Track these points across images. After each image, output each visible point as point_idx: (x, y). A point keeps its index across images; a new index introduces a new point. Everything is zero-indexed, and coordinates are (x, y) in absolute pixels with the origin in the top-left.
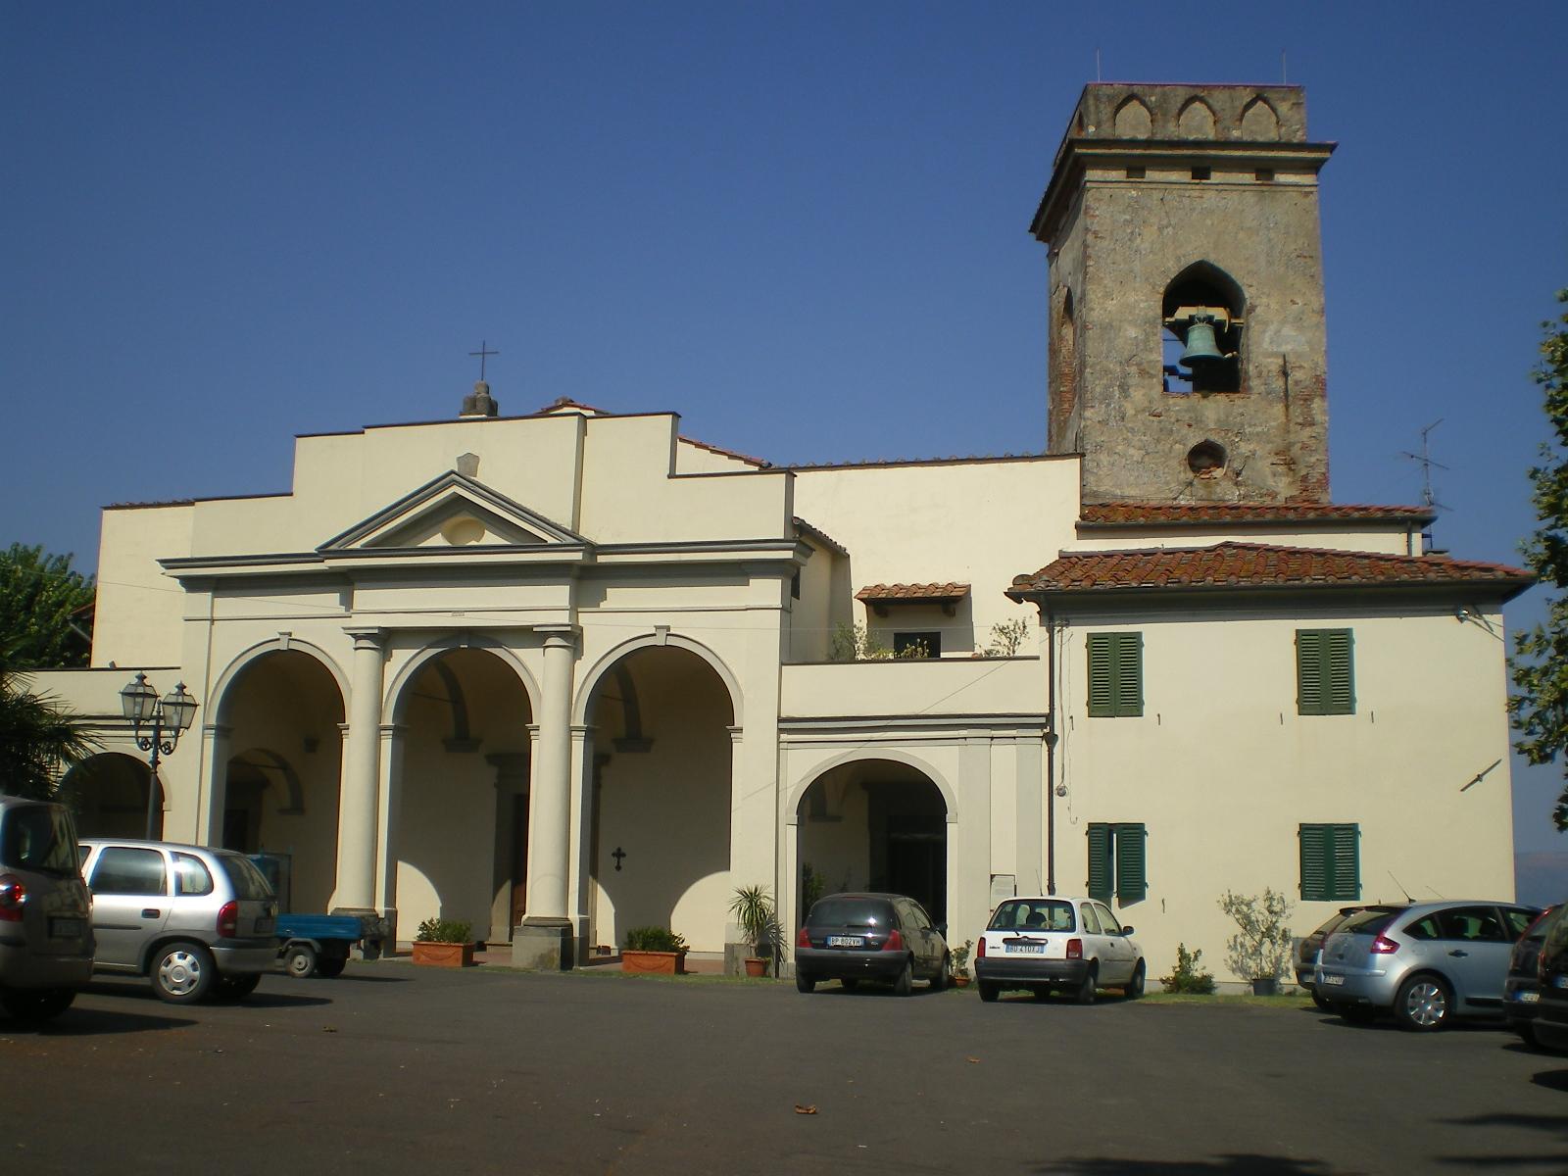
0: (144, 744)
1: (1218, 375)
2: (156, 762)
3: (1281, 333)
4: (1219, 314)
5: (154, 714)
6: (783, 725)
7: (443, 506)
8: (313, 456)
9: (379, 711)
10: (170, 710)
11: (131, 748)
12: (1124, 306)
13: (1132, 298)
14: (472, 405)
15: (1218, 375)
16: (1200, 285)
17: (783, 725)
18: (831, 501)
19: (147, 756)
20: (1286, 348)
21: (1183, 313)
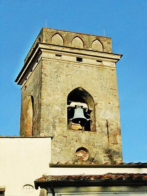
1: (86, 125)
4: (85, 106)
12: (55, 101)
15: (86, 125)
16: (78, 95)
20: (107, 118)
21: (73, 104)
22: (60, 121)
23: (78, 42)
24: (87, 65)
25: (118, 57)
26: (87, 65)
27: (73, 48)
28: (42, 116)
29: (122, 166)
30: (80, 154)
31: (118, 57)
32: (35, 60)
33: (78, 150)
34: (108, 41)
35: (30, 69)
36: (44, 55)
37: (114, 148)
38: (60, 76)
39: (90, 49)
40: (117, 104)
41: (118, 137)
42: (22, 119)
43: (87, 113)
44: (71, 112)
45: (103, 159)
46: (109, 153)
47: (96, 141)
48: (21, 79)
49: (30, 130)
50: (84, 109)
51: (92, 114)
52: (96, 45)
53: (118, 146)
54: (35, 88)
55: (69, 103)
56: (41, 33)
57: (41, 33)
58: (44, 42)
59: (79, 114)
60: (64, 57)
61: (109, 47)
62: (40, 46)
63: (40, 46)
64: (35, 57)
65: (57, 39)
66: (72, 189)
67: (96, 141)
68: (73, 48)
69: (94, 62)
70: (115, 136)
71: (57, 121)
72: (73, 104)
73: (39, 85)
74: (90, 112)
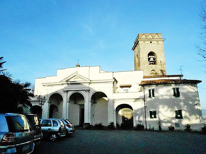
0: (40, 104)
1: (154, 63)
2: (41, 106)
3: (160, 58)
4: (153, 57)
5: (41, 100)
6: (151, 91)
7: (195, 124)
8: (59, 72)
9: (89, 99)
10: (43, 100)
11: (38, 105)
12: (144, 56)
13: (144, 55)
14: (77, 66)
15: (154, 63)
16: (151, 54)
17: (151, 91)
18: (117, 76)
19: (40, 106)
20: (161, 60)
21: (150, 57)
22: (146, 63)
23: (150, 37)
24: (154, 44)
25: (164, 40)
26: (154, 44)
27: (148, 39)
28: (140, 61)
29: (166, 76)
30: (153, 72)
31: (164, 40)
32: (137, 44)
33: (152, 71)
34: (160, 34)
35: (136, 46)
36: (140, 42)
37: (163, 69)
38: (145, 48)
39: (154, 38)
40: (164, 55)
41: (164, 65)
42: (135, 61)
43: (154, 59)
44: (149, 59)
45: (160, 74)
46: (162, 71)
47: (157, 68)
48: (134, 49)
49: (137, 66)
50: (153, 58)
51: (156, 59)
52: (156, 37)
53: (164, 68)
54: (138, 53)
55: (148, 56)
56: (138, 35)
57: (138, 35)
58: (139, 38)
59: (152, 59)
60: (146, 42)
61: (161, 37)
62: (138, 40)
63: (138, 40)
64: (136, 43)
65: (144, 37)
66: (148, 86)
67: (157, 68)
68: (148, 39)
69: (156, 42)
70: (163, 65)
71: (145, 62)
72: (150, 57)
73: (139, 52)
74: (155, 58)
